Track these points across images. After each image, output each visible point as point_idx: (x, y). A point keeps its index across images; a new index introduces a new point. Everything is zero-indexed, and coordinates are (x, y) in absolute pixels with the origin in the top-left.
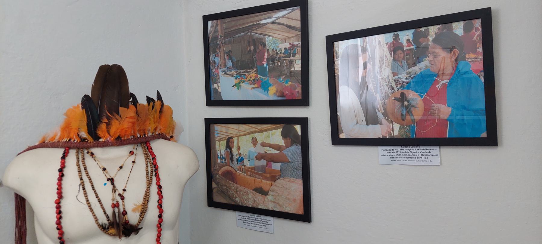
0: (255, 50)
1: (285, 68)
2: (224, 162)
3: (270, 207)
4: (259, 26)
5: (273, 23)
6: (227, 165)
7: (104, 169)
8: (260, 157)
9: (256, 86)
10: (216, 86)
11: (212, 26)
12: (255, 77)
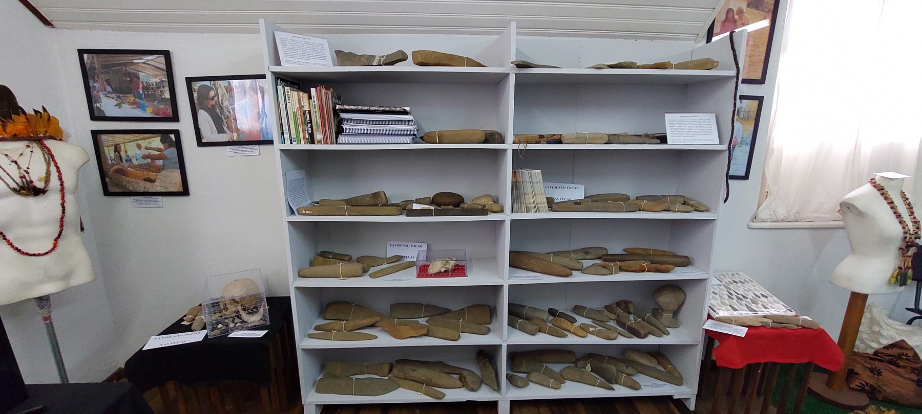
0: (131, 81)
1: (158, 95)
2: (115, 162)
3: (159, 189)
4: (133, 64)
5: (144, 63)
6: (117, 165)
7: (7, 155)
8: (145, 157)
9: (135, 106)
10: (98, 105)
11: (88, 59)
12: (133, 100)
